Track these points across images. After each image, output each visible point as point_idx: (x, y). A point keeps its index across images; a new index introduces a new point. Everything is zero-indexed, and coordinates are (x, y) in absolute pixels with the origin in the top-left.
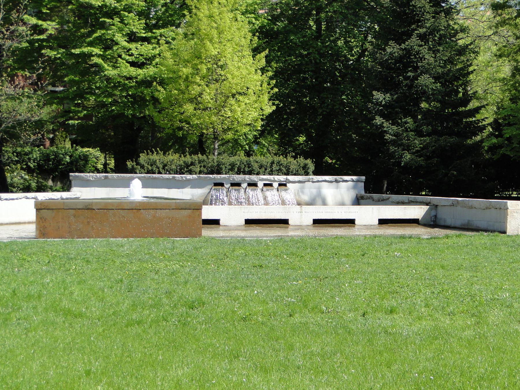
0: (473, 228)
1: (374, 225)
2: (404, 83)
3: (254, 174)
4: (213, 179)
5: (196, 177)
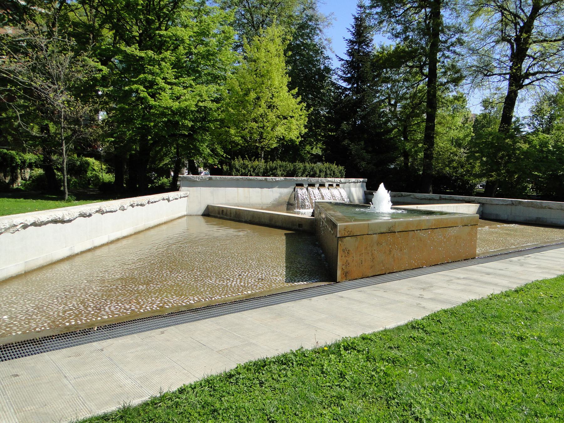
0: (501, 218)
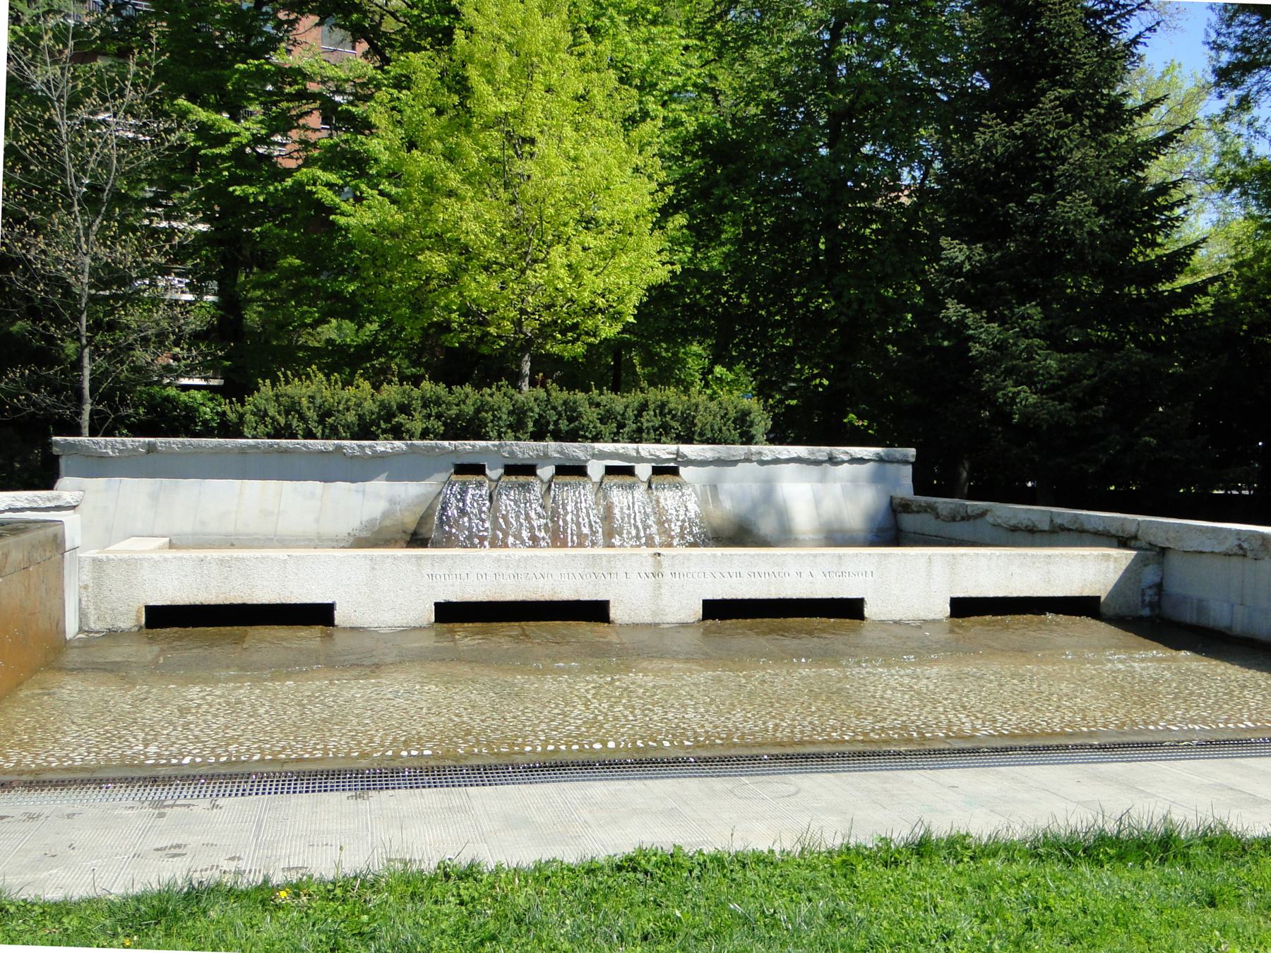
1: (934, 621)
2: (1017, 220)
3: (585, 438)
4: (452, 452)
5: (404, 447)
